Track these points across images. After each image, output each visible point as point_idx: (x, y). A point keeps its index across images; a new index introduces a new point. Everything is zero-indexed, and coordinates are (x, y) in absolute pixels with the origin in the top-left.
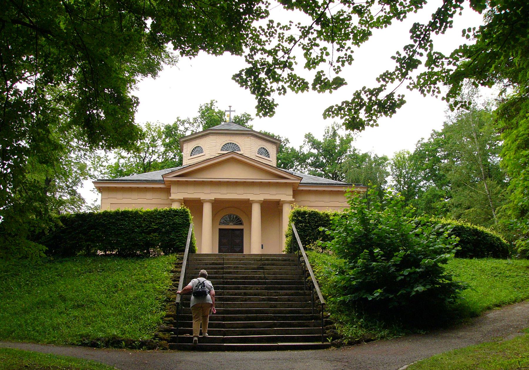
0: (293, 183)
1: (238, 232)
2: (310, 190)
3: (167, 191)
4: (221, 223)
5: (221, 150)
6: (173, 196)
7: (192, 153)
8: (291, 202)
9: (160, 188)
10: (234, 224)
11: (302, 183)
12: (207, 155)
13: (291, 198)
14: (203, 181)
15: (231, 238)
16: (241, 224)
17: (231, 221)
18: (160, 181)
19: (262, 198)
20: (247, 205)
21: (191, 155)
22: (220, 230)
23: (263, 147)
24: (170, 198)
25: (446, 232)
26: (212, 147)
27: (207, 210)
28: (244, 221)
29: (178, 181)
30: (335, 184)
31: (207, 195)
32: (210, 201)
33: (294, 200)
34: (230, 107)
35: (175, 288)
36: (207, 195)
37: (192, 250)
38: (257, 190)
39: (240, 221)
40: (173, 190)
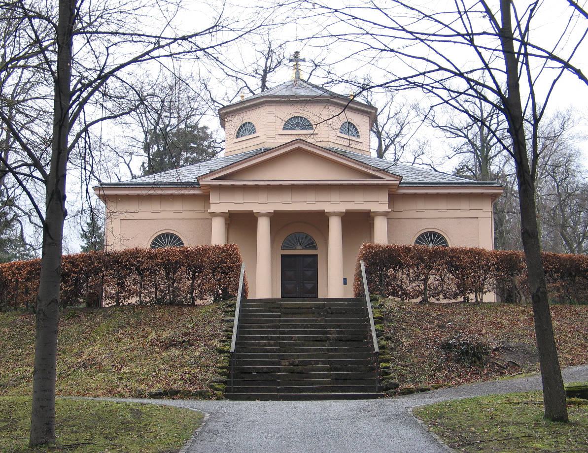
0: (389, 185)
1: (309, 260)
2: (415, 194)
3: (205, 198)
5: (284, 129)
6: (214, 209)
7: (238, 133)
8: (385, 214)
9: (194, 195)
10: (304, 248)
11: (404, 183)
12: (262, 137)
13: (385, 208)
15: (299, 272)
17: (249, 356)
19: (342, 208)
20: (320, 219)
21: (237, 137)
22: (283, 256)
24: (209, 211)
25: (542, 289)
26: (270, 129)
27: (263, 227)
28: (319, 242)
29: (220, 185)
30: (455, 183)
31: (263, 205)
36: (263, 205)
37: (245, 292)
39: (313, 243)
40: (214, 198)
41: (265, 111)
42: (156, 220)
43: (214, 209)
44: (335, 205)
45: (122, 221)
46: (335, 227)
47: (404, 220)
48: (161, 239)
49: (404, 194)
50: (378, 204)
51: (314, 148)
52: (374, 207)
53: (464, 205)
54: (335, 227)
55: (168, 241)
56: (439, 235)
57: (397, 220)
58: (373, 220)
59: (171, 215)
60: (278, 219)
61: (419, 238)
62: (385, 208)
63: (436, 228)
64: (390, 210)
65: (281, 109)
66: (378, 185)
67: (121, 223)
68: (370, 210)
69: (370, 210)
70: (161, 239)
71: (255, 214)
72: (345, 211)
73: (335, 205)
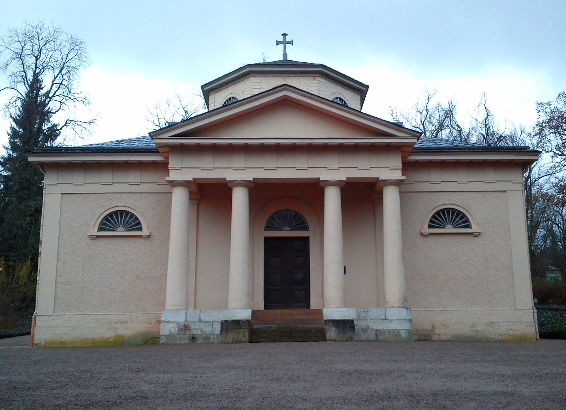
3: (163, 167)
8: (398, 183)
10: (292, 230)
13: (397, 175)
16: (306, 228)
20: (313, 191)
22: (266, 239)
24: (167, 179)
27: (240, 200)
31: (238, 171)
34: (285, 35)
36: (238, 171)
39: (303, 223)
40: (173, 162)
41: (249, 82)
42: (106, 195)
43: (174, 176)
44: (333, 171)
45: (64, 196)
46: (332, 200)
47: (414, 194)
48: (440, 216)
50: (387, 169)
51: (305, 96)
52: (384, 175)
53: (490, 176)
54: (332, 200)
55: (121, 220)
56: (459, 213)
57: (408, 194)
60: (259, 191)
61: (434, 217)
62: (397, 175)
63: (455, 203)
64: (404, 178)
65: (267, 80)
70: (440, 216)
71: (229, 185)
73: (333, 171)
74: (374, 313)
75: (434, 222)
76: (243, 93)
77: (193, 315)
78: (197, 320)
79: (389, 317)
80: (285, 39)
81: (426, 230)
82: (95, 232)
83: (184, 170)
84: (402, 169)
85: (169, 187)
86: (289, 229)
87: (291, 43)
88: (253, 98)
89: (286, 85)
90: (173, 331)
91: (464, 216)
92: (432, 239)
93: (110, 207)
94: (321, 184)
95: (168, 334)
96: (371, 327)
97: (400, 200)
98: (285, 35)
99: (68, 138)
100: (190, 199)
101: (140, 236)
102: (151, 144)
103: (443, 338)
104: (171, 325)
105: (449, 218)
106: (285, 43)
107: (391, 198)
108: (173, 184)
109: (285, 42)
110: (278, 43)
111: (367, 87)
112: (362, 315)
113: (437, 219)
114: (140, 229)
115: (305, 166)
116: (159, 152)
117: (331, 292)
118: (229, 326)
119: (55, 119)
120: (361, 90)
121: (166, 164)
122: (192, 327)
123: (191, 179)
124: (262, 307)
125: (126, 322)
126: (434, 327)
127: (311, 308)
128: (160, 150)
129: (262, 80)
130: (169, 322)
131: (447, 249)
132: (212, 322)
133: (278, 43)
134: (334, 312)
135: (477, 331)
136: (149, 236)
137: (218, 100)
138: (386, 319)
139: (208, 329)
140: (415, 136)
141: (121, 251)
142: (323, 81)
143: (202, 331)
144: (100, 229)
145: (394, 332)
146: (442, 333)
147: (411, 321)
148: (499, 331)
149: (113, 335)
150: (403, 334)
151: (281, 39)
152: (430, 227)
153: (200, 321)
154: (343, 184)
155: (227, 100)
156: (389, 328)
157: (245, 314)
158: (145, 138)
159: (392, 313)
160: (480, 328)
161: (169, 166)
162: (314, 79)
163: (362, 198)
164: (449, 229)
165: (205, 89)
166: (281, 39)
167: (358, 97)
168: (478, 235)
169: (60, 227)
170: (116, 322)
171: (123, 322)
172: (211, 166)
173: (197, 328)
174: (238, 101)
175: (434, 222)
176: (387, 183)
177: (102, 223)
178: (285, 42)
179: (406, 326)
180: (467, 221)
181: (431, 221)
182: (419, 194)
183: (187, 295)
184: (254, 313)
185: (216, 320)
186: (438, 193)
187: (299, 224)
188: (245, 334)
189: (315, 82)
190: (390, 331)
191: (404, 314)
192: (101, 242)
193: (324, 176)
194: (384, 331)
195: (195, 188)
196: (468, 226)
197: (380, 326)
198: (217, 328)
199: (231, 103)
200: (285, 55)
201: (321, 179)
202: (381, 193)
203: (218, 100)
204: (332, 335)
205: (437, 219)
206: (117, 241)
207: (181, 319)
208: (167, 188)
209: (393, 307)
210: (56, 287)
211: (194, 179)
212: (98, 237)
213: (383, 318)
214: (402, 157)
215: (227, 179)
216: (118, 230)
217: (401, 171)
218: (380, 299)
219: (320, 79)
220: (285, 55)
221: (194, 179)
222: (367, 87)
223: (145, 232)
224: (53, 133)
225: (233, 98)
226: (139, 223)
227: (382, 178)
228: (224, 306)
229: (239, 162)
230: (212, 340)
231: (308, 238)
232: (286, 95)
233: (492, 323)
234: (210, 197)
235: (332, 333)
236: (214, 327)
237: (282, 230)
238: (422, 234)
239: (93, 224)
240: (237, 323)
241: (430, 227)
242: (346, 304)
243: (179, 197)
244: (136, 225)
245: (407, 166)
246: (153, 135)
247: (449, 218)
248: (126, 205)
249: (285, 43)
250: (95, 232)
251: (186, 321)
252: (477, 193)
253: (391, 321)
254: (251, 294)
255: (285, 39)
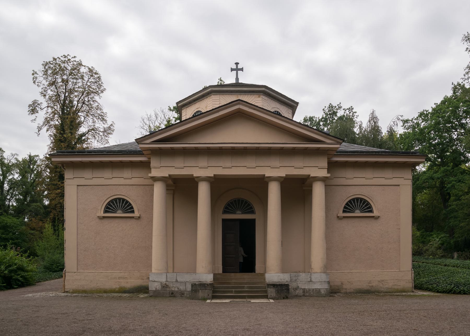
3: (146, 166)
4: (225, 212)
8: (323, 180)
10: (242, 213)
13: (324, 173)
14: (196, 149)
16: (253, 212)
18: (300, 123)
20: (261, 183)
22: (223, 220)
23: (277, 110)
24: (150, 175)
27: (204, 191)
28: (257, 208)
29: (160, 149)
32: (207, 179)
33: (329, 175)
34: (237, 64)
35: (59, 191)
36: (202, 169)
38: (275, 162)
39: (251, 208)
40: (154, 163)
43: (155, 173)
44: (275, 169)
45: (79, 187)
48: (352, 204)
49: (336, 162)
50: (316, 169)
51: (254, 109)
53: (388, 173)
58: (311, 186)
59: (122, 181)
60: (216, 183)
62: (324, 173)
64: (329, 175)
66: (318, 149)
67: (77, 189)
68: (310, 175)
69: (310, 175)
70: (352, 204)
71: (196, 179)
72: (285, 176)
74: (303, 276)
75: (347, 208)
76: (206, 107)
77: (172, 277)
78: (174, 281)
79: (313, 280)
80: (237, 66)
81: (341, 214)
82: (102, 214)
83: (162, 169)
84: (328, 169)
85: (151, 180)
86: (241, 213)
87: (242, 69)
88: (214, 111)
89: (239, 100)
90: (158, 288)
91: (368, 203)
92: (345, 222)
93: (112, 195)
94: (266, 180)
95: (154, 289)
96: (300, 287)
97: (325, 193)
98: (237, 64)
99: (95, 144)
100: (167, 190)
101: (133, 217)
102: (139, 147)
103: (348, 291)
104: (156, 284)
105: (359, 206)
106: (237, 70)
107: (318, 191)
108: (155, 179)
109: (237, 69)
110: (232, 70)
111: (297, 103)
112: (294, 279)
113: (349, 206)
114: (133, 212)
115: (254, 165)
116: (143, 154)
117: (272, 262)
118: (198, 287)
119: (83, 130)
120: (292, 105)
121: (149, 163)
122: (171, 285)
123: (167, 176)
124: (221, 271)
125: (126, 278)
126: (342, 284)
127: (256, 272)
128: (144, 152)
129: (221, 97)
130: (155, 281)
131: (355, 230)
132: (185, 283)
133: (232, 70)
134: (274, 275)
135: (372, 286)
136: (139, 217)
137: (188, 113)
138: (311, 281)
139: (182, 288)
140: (338, 142)
141: (120, 230)
142: (266, 98)
143: (178, 289)
144: (106, 212)
145: (316, 290)
146: (348, 287)
147: (329, 282)
148: (387, 286)
149: (118, 286)
150: (323, 292)
151: (234, 67)
152: (344, 211)
153: (177, 281)
154: (282, 180)
155: (195, 113)
156: (313, 288)
157: (209, 278)
158: (133, 143)
159: (315, 277)
160: (374, 284)
161: (151, 165)
162: (259, 97)
163: (297, 192)
164: (358, 213)
165: (179, 105)
166: (234, 67)
167: (290, 111)
168: (376, 218)
169: (77, 210)
170: (119, 278)
171: (124, 278)
172: (182, 165)
173: (174, 286)
174: (203, 113)
175: (347, 208)
176: (316, 179)
177: (107, 207)
178: (237, 69)
179: (326, 286)
180: (370, 207)
181: (345, 207)
182: (338, 187)
183: (167, 263)
184: (215, 275)
185: (188, 281)
186: (351, 187)
187: (248, 209)
188: (208, 292)
189: (260, 99)
190: (313, 290)
191: (324, 277)
192: (106, 221)
193: (269, 173)
194: (309, 290)
195: (170, 182)
196: (371, 211)
197: (307, 287)
198: (189, 288)
199: (198, 115)
200: (237, 79)
201: (266, 176)
202: (311, 186)
203: (188, 113)
204: (272, 295)
205: (349, 206)
206: (117, 221)
207: (163, 280)
208: (149, 182)
209: (317, 273)
210: (77, 253)
211: (169, 175)
212: (104, 217)
213: (309, 280)
214: (328, 159)
215: (194, 176)
216: (118, 212)
217: (326, 170)
218: (307, 267)
219: (264, 97)
220: (237, 79)
221: (169, 175)
222: (297, 103)
223: (136, 214)
224: (80, 140)
225: (199, 111)
226: (132, 208)
227: (312, 175)
228: (193, 270)
229: (203, 162)
230: (185, 295)
231: (254, 221)
232: (239, 108)
233: (383, 281)
234: (181, 190)
235: (272, 292)
236: (187, 286)
237: (235, 213)
238: (338, 217)
239: (100, 207)
240: (203, 285)
241: (344, 211)
242: (283, 270)
243: (159, 190)
244: (130, 209)
245: (332, 166)
246: (138, 141)
247: (359, 206)
248: (122, 194)
249: (237, 70)
250: (102, 214)
251: (167, 281)
252: (379, 186)
253: (314, 283)
254: (213, 262)
255: (237, 66)
